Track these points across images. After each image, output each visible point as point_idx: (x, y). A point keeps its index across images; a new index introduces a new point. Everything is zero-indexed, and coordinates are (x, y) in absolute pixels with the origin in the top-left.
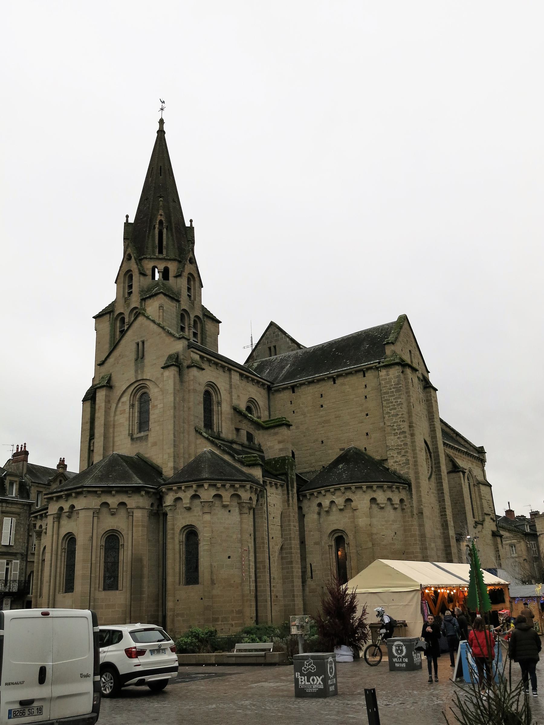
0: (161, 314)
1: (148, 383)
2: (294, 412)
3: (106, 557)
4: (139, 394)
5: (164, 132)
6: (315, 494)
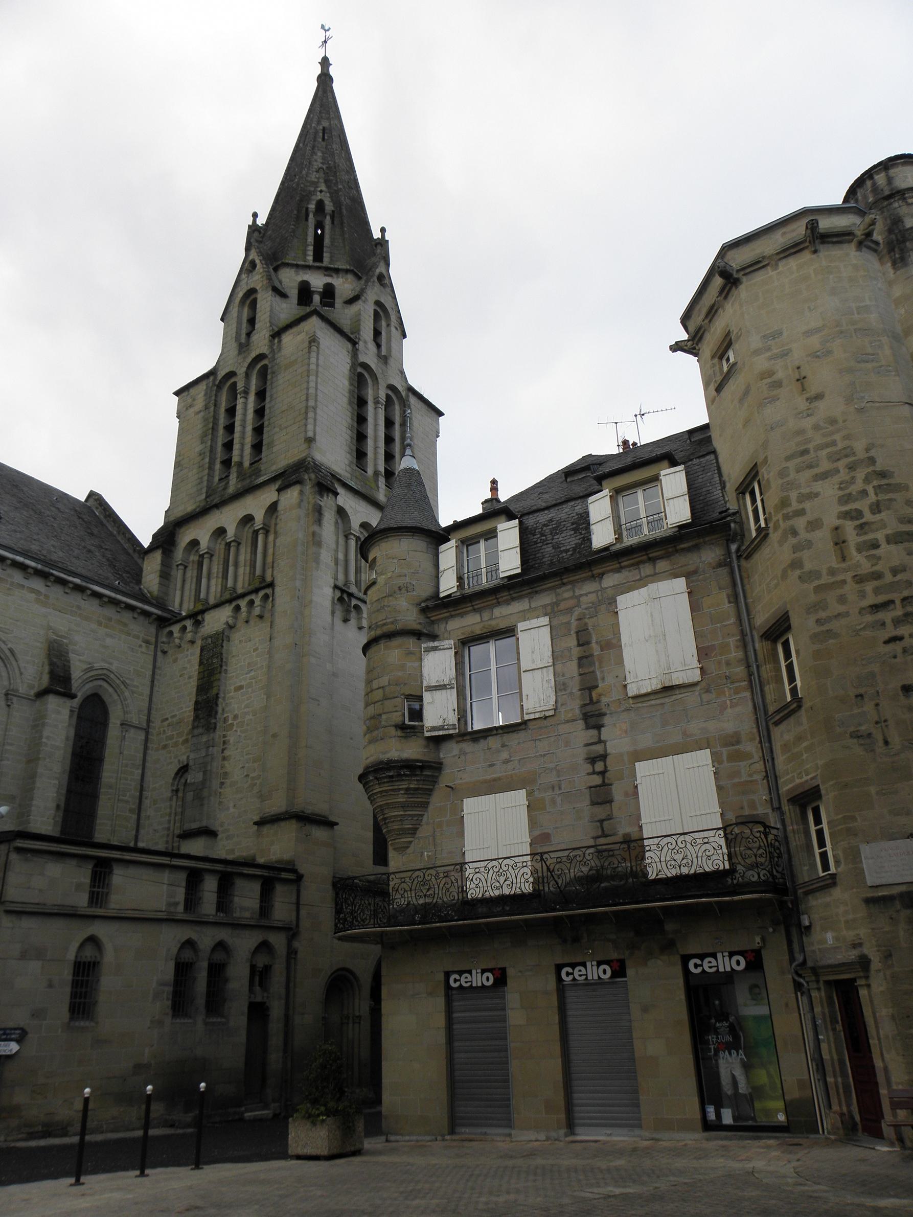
5: (331, 79)
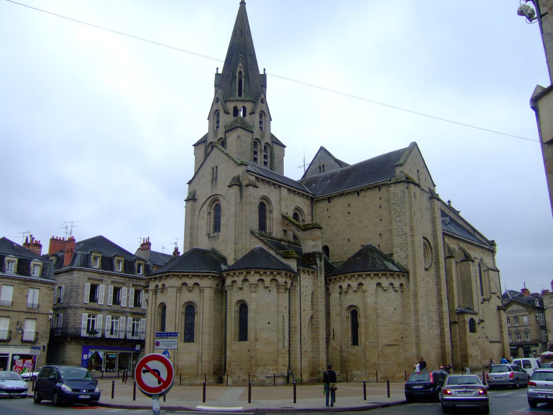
0: (239, 143)
1: (219, 197)
2: (329, 217)
3: (186, 320)
4: (214, 205)
5: (245, 4)
6: (338, 279)
